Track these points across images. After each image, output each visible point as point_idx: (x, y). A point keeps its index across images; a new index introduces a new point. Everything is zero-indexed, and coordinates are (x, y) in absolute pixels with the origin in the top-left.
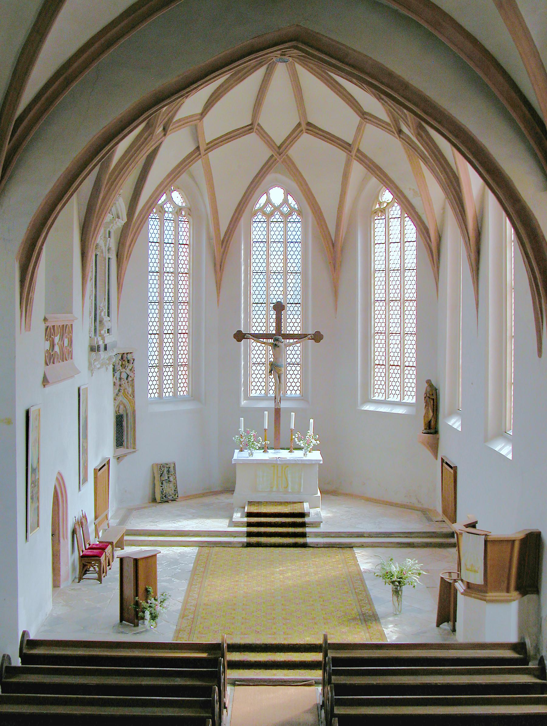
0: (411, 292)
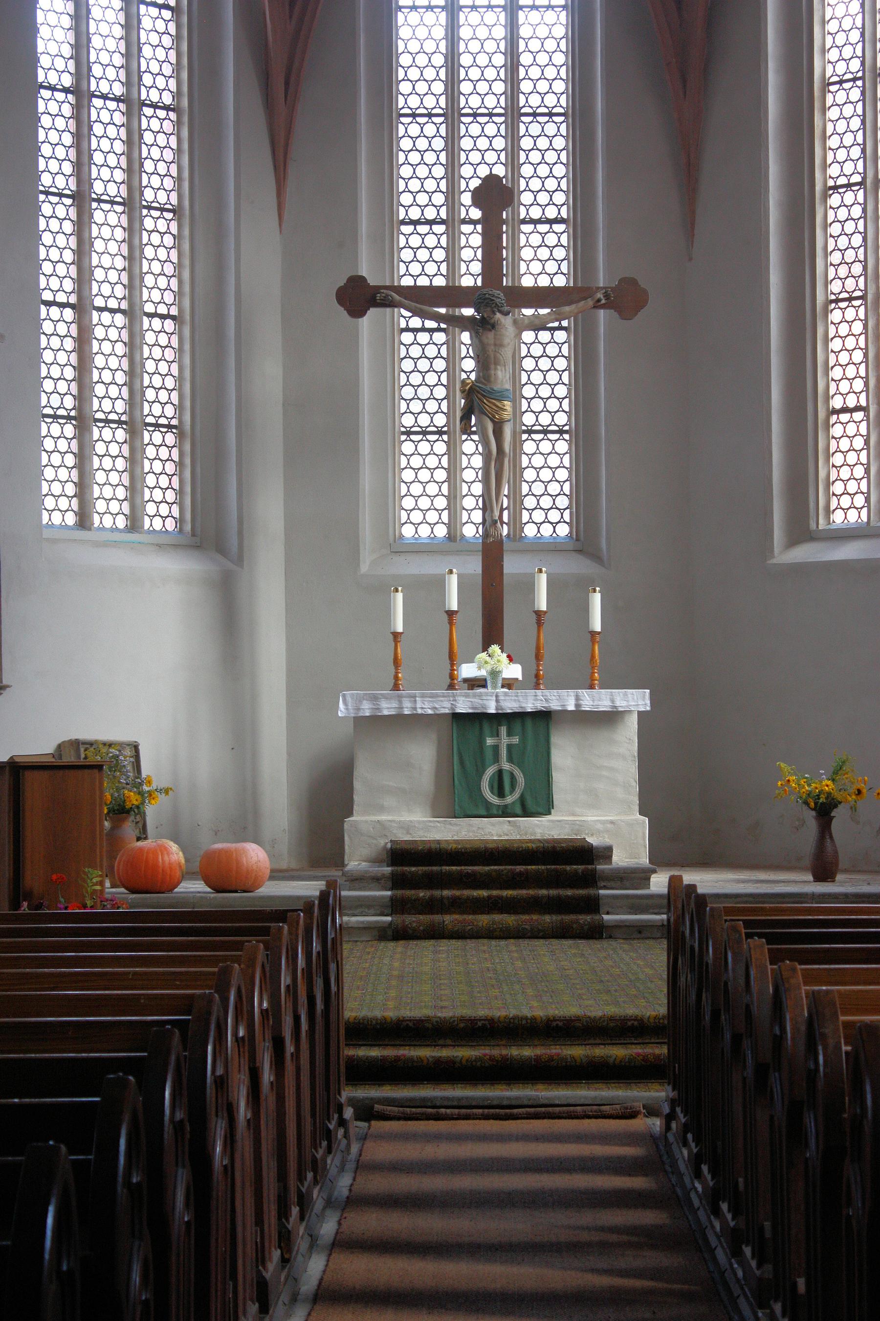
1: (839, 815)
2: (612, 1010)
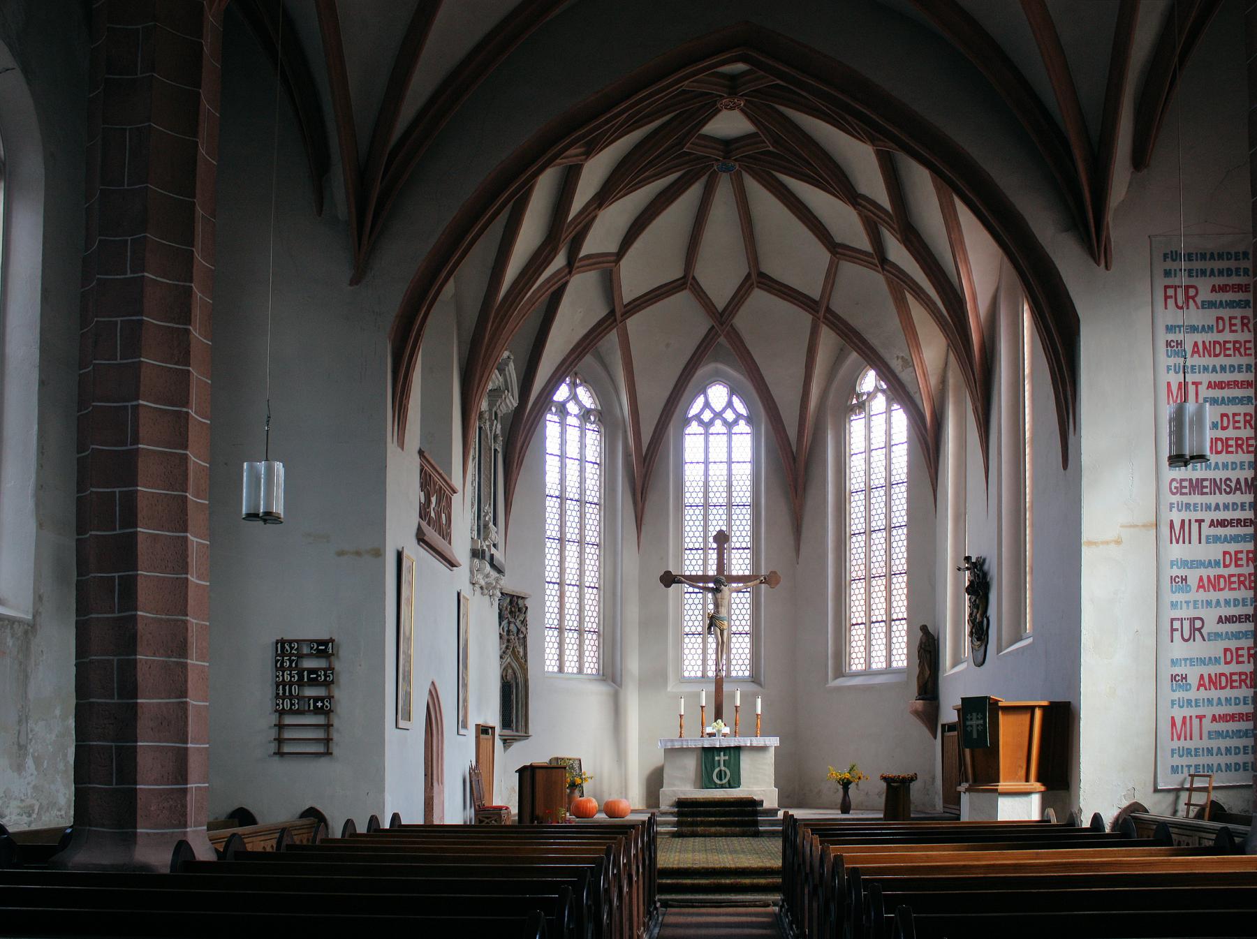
0: (900, 515)
1: (852, 787)
2: (760, 865)
